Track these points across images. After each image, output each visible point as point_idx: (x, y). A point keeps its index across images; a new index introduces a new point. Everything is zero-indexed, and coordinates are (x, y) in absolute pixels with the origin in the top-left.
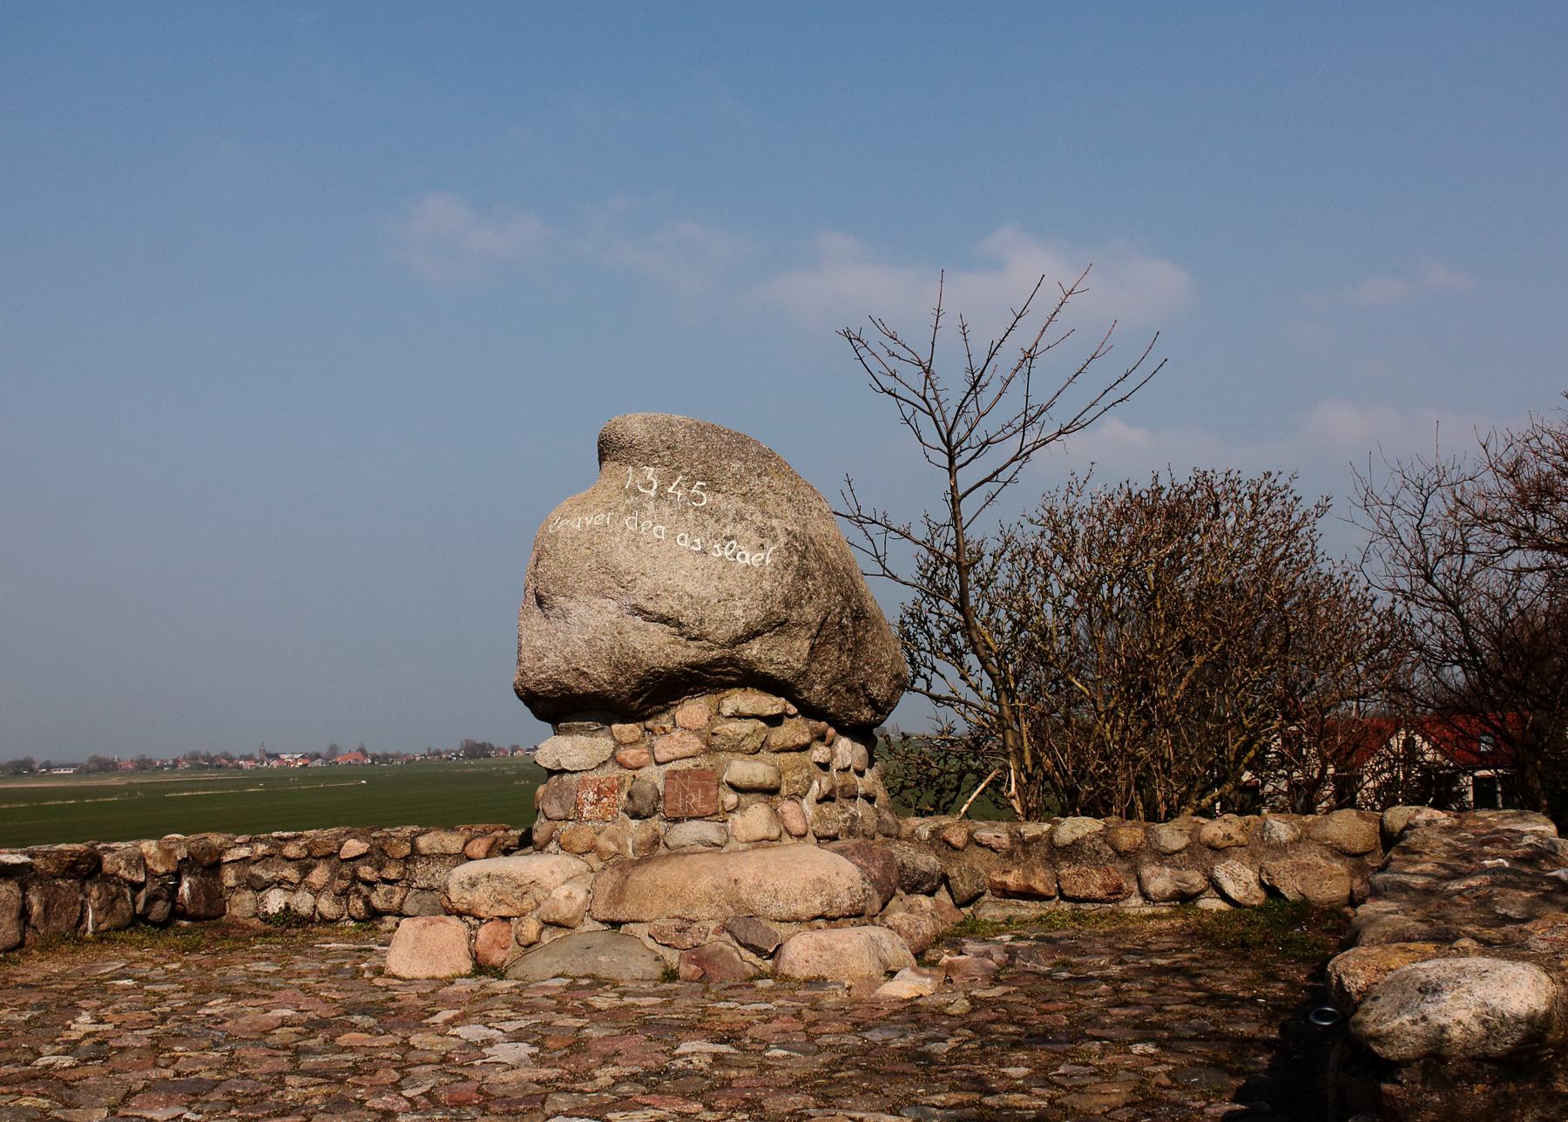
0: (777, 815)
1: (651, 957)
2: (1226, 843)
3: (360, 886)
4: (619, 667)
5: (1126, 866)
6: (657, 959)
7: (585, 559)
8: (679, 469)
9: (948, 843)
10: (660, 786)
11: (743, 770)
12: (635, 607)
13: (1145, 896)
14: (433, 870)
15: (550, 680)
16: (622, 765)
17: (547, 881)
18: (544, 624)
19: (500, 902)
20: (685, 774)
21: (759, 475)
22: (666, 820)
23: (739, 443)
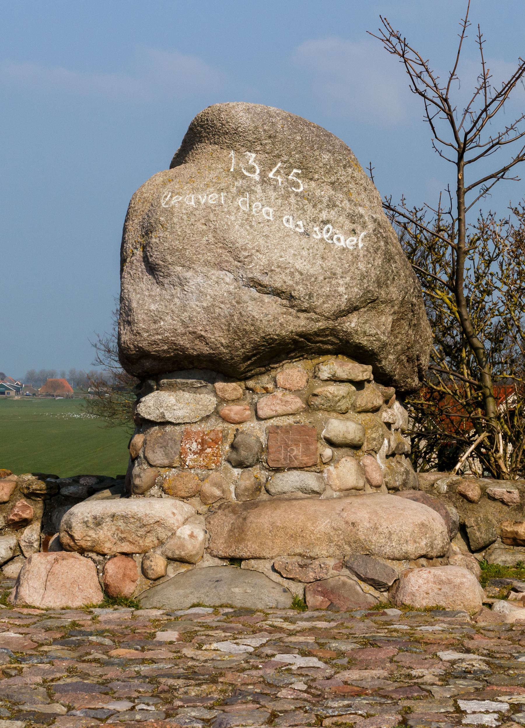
0: (362, 470)
1: (279, 589)
6: (285, 591)
7: (203, 234)
8: (279, 156)
10: (263, 439)
11: (339, 427)
12: (252, 280)
15: (165, 341)
16: (225, 419)
17: (172, 521)
18: (157, 290)
19: (122, 539)
20: (287, 430)
21: (345, 167)
22: (270, 469)
23: (324, 139)
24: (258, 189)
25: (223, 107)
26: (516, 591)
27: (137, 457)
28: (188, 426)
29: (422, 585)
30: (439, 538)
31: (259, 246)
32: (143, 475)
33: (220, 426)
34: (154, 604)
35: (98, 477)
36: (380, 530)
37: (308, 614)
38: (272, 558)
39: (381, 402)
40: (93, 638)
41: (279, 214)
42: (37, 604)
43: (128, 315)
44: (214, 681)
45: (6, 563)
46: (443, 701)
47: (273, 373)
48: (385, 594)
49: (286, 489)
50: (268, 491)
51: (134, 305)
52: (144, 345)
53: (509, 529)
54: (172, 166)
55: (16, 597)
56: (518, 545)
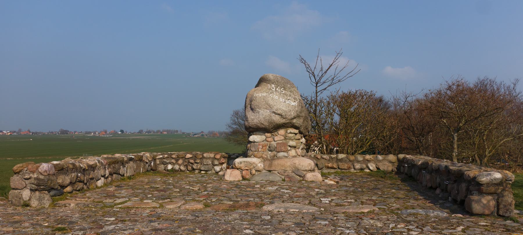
0: (296, 152)
4: (270, 123)
11: (292, 143)
13: (355, 169)
16: (267, 141)
20: (281, 143)
23: (288, 82)
32: (250, 153)
33: (266, 143)
44: (269, 194)
46: (317, 198)
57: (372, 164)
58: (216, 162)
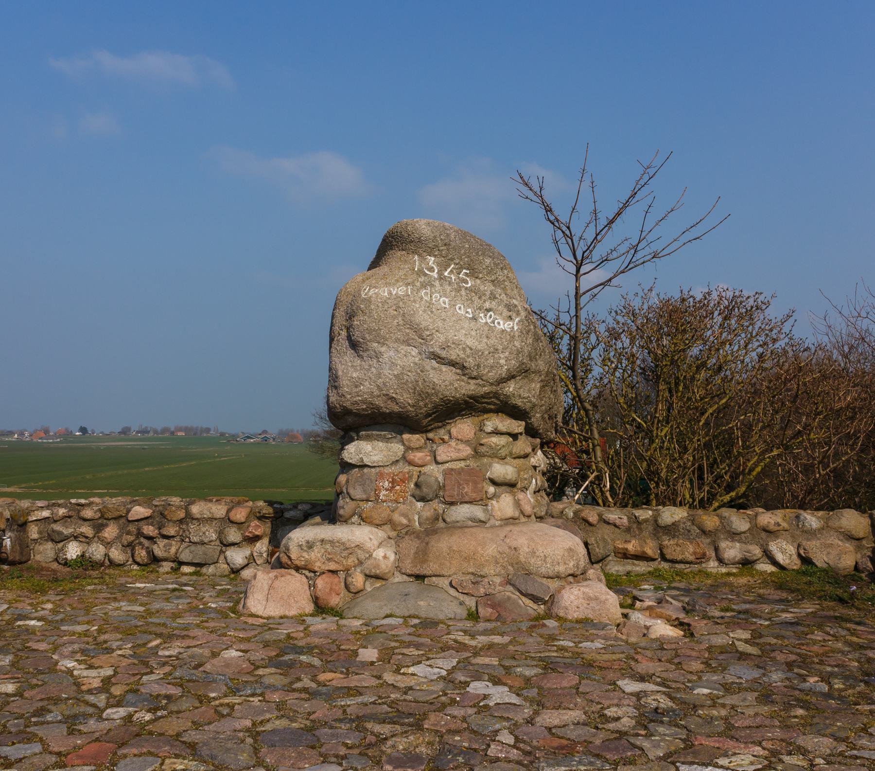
0: (517, 504)
1: (456, 602)
2: (777, 528)
3: (142, 540)
5: (708, 541)
7: (394, 317)
8: (452, 259)
9: (586, 521)
10: (441, 479)
11: (501, 470)
12: (433, 353)
13: (721, 561)
14: (204, 529)
15: (364, 402)
16: (411, 463)
17: (369, 545)
18: (358, 362)
19: (329, 560)
20: (459, 472)
22: (445, 503)
23: (486, 249)
24: (437, 283)
25: (409, 221)
26: (641, 601)
27: (341, 492)
28: (382, 469)
29: (573, 600)
30: (582, 559)
31: (438, 327)
32: (345, 506)
33: (407, 468)
34: (355, 614)
35: (311, 504)
36: (537, 554)
37: (482, 626)
38: (450, 576)
39: (530, 450)
40: (303, 658)
41: (453, 303)
42: (260, 613)
43: (335, 382)
45: (243, 568)
47: (448, 427)
48: (542, 606)
49: (458, 519)
50: (444, 520)
51: (340, 373)
52: (348, 404)
53: (620, 546)
54: (369, 269)
55: (243, 607)
56: (627, 558)
57: (784, 544)
58: (233, 535)
